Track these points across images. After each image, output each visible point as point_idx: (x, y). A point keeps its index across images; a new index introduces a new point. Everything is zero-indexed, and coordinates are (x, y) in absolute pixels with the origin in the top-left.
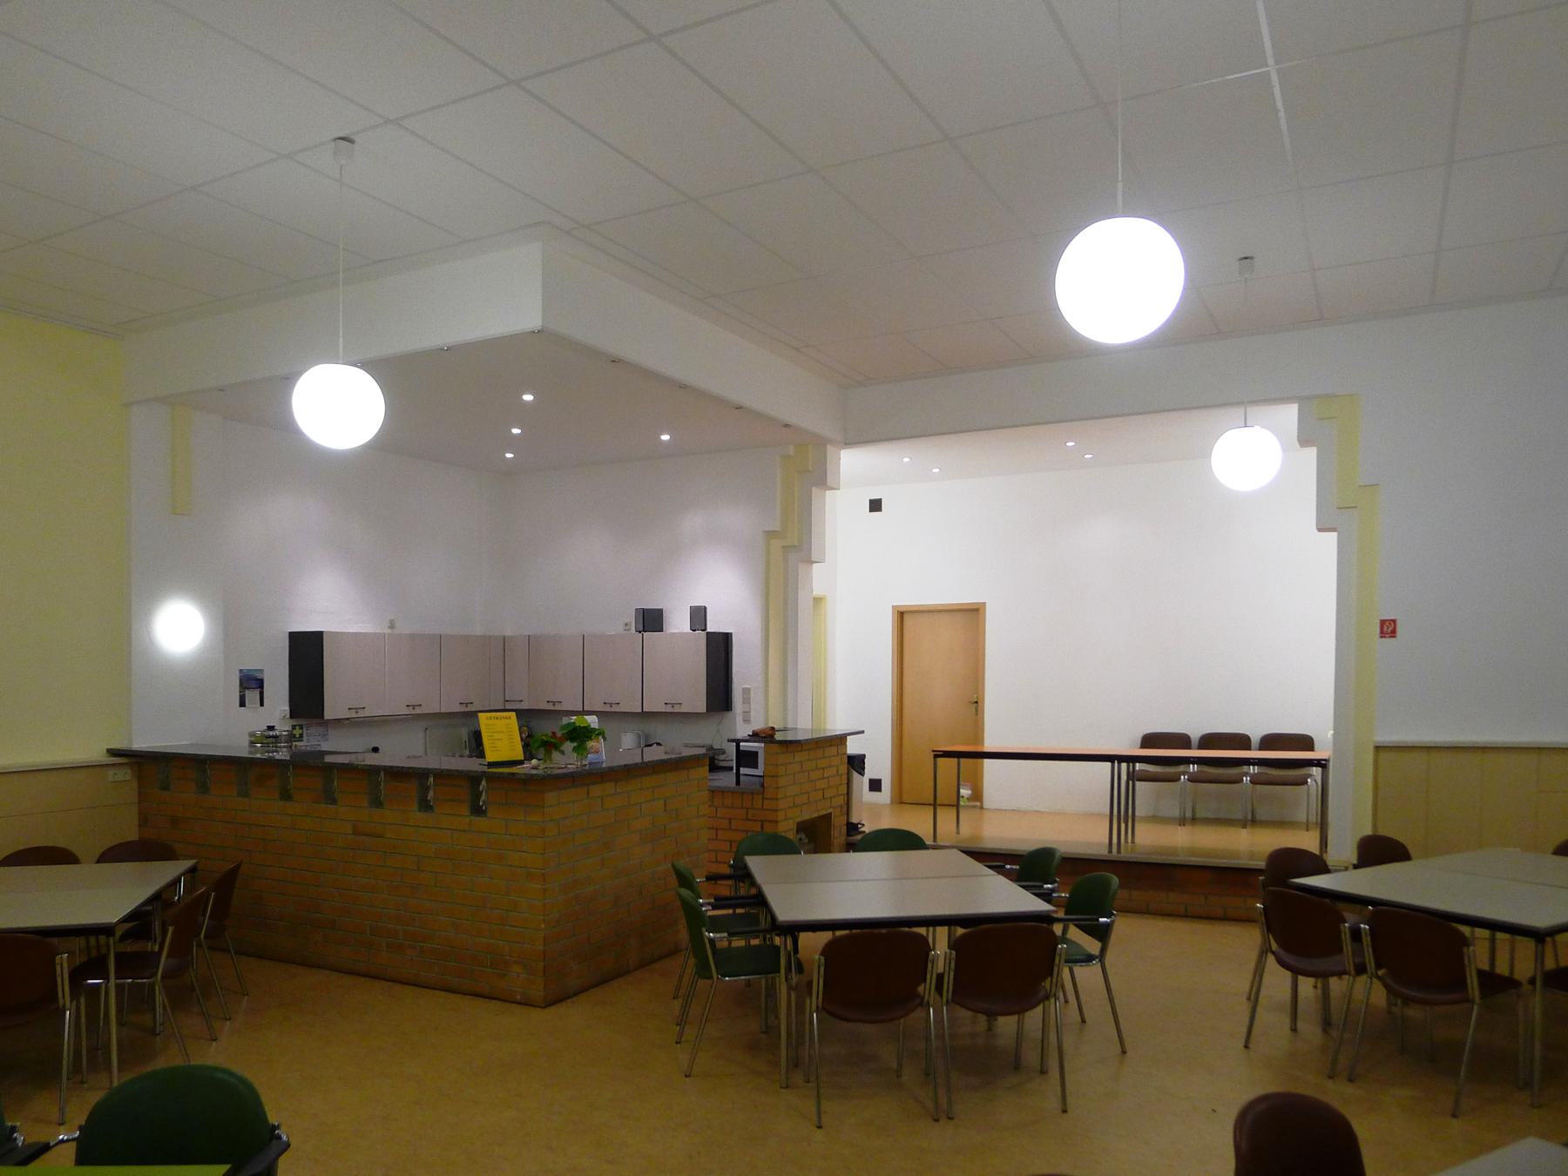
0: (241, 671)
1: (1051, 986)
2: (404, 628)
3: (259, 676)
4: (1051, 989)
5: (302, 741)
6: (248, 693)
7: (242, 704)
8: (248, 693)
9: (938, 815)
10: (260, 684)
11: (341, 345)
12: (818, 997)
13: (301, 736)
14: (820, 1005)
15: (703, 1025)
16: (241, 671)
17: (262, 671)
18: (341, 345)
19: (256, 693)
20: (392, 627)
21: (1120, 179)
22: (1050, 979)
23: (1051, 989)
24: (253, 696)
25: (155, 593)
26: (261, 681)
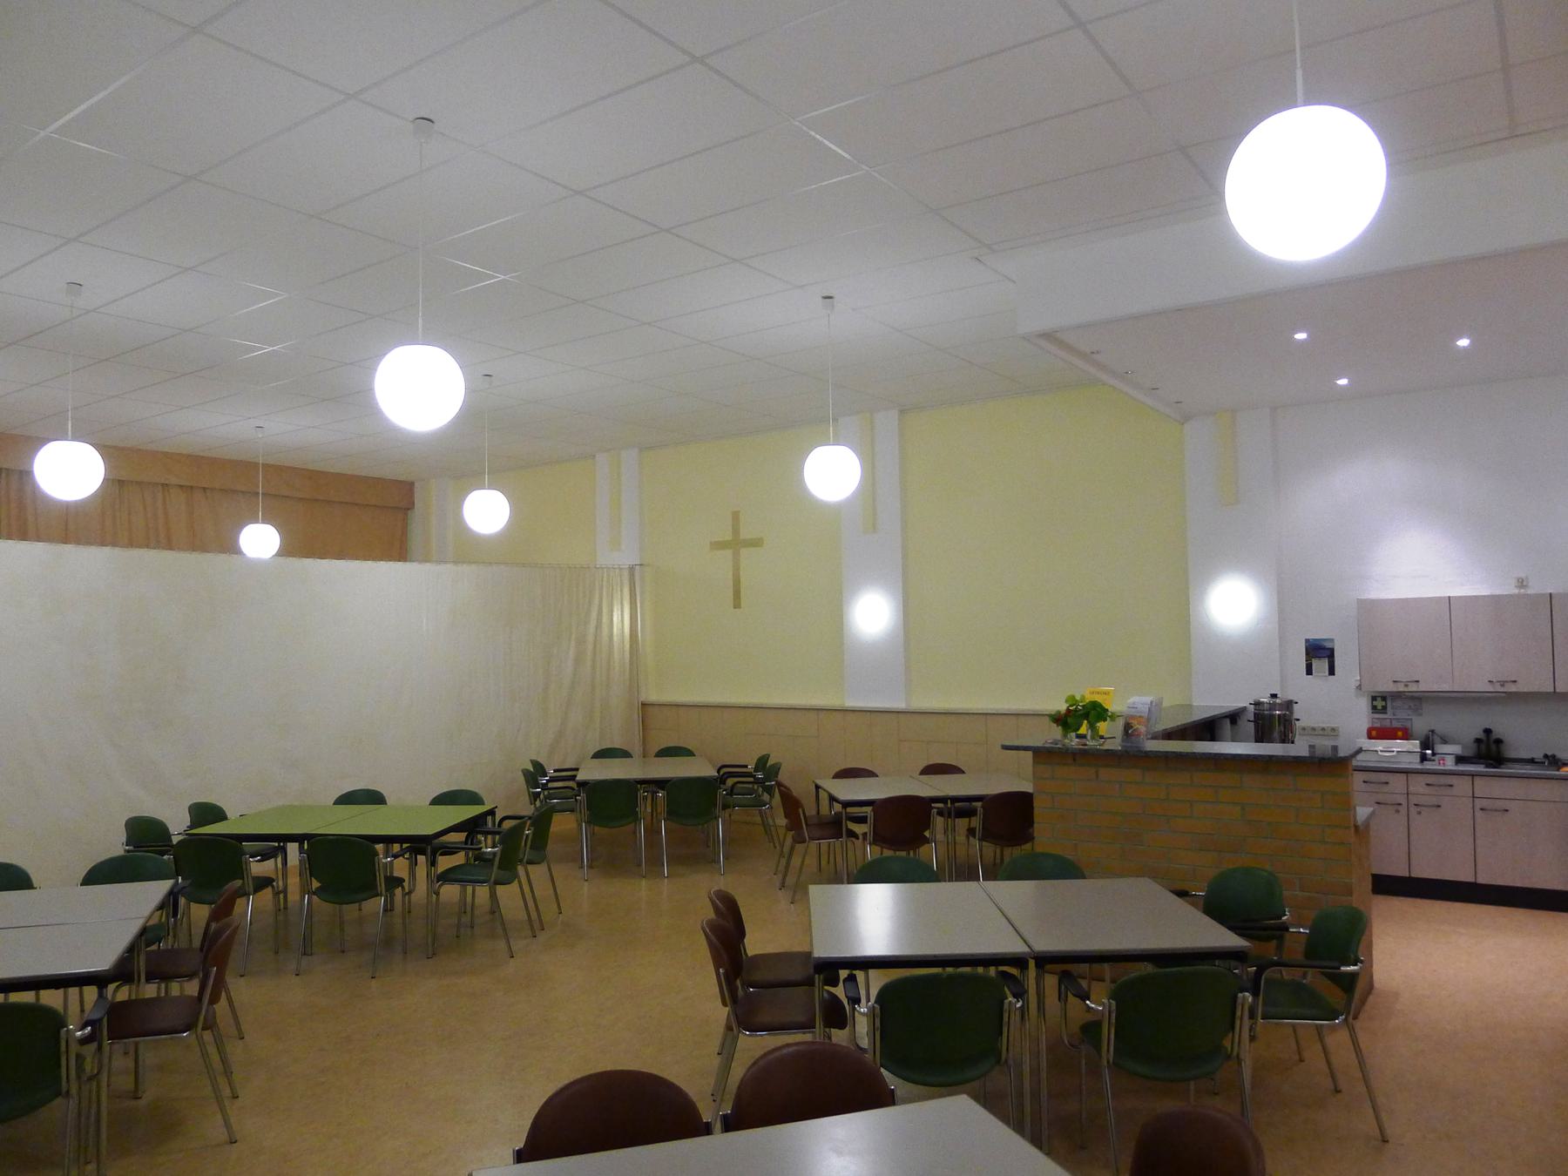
0: (1307, 641)
1: (1232, 1044)
2: (1535, 588)
3: (1328, 645)
4: (1232, 1048)
5: (1386, 713)
6: (1315, 663)
7: (1309, 671)
8: (1315, 663)
9: (1475, 783)
10: (1329, 654)
11: (420, 326)
12: (1108, 1050)
13: (1384, 708)
14: (1111, 1060)
15: (215, 1057)
16: (1307, 641)
17: (1332, 640)
18: (420, 326)
19: (1325, 664)
20: (1522, 583)
21: (1299, 65)
22: (1230, 1035)
23: (1232, 1048)
24: (1321, 665)
25: (1210, 572)
26: (1332, 651)
